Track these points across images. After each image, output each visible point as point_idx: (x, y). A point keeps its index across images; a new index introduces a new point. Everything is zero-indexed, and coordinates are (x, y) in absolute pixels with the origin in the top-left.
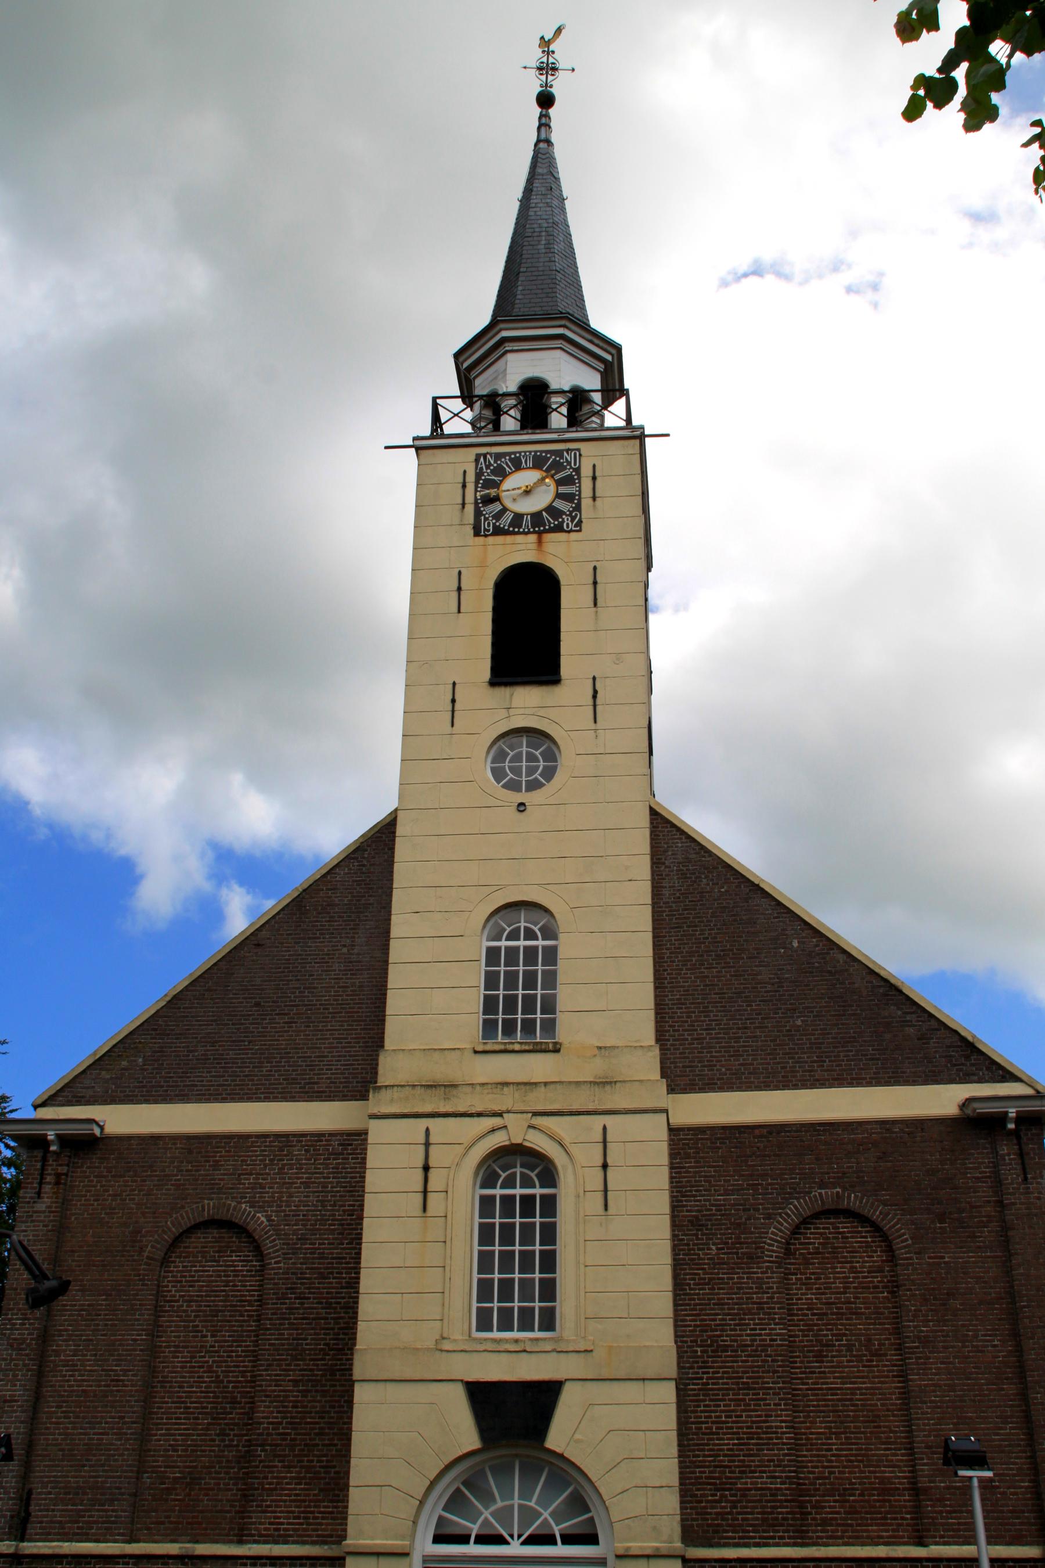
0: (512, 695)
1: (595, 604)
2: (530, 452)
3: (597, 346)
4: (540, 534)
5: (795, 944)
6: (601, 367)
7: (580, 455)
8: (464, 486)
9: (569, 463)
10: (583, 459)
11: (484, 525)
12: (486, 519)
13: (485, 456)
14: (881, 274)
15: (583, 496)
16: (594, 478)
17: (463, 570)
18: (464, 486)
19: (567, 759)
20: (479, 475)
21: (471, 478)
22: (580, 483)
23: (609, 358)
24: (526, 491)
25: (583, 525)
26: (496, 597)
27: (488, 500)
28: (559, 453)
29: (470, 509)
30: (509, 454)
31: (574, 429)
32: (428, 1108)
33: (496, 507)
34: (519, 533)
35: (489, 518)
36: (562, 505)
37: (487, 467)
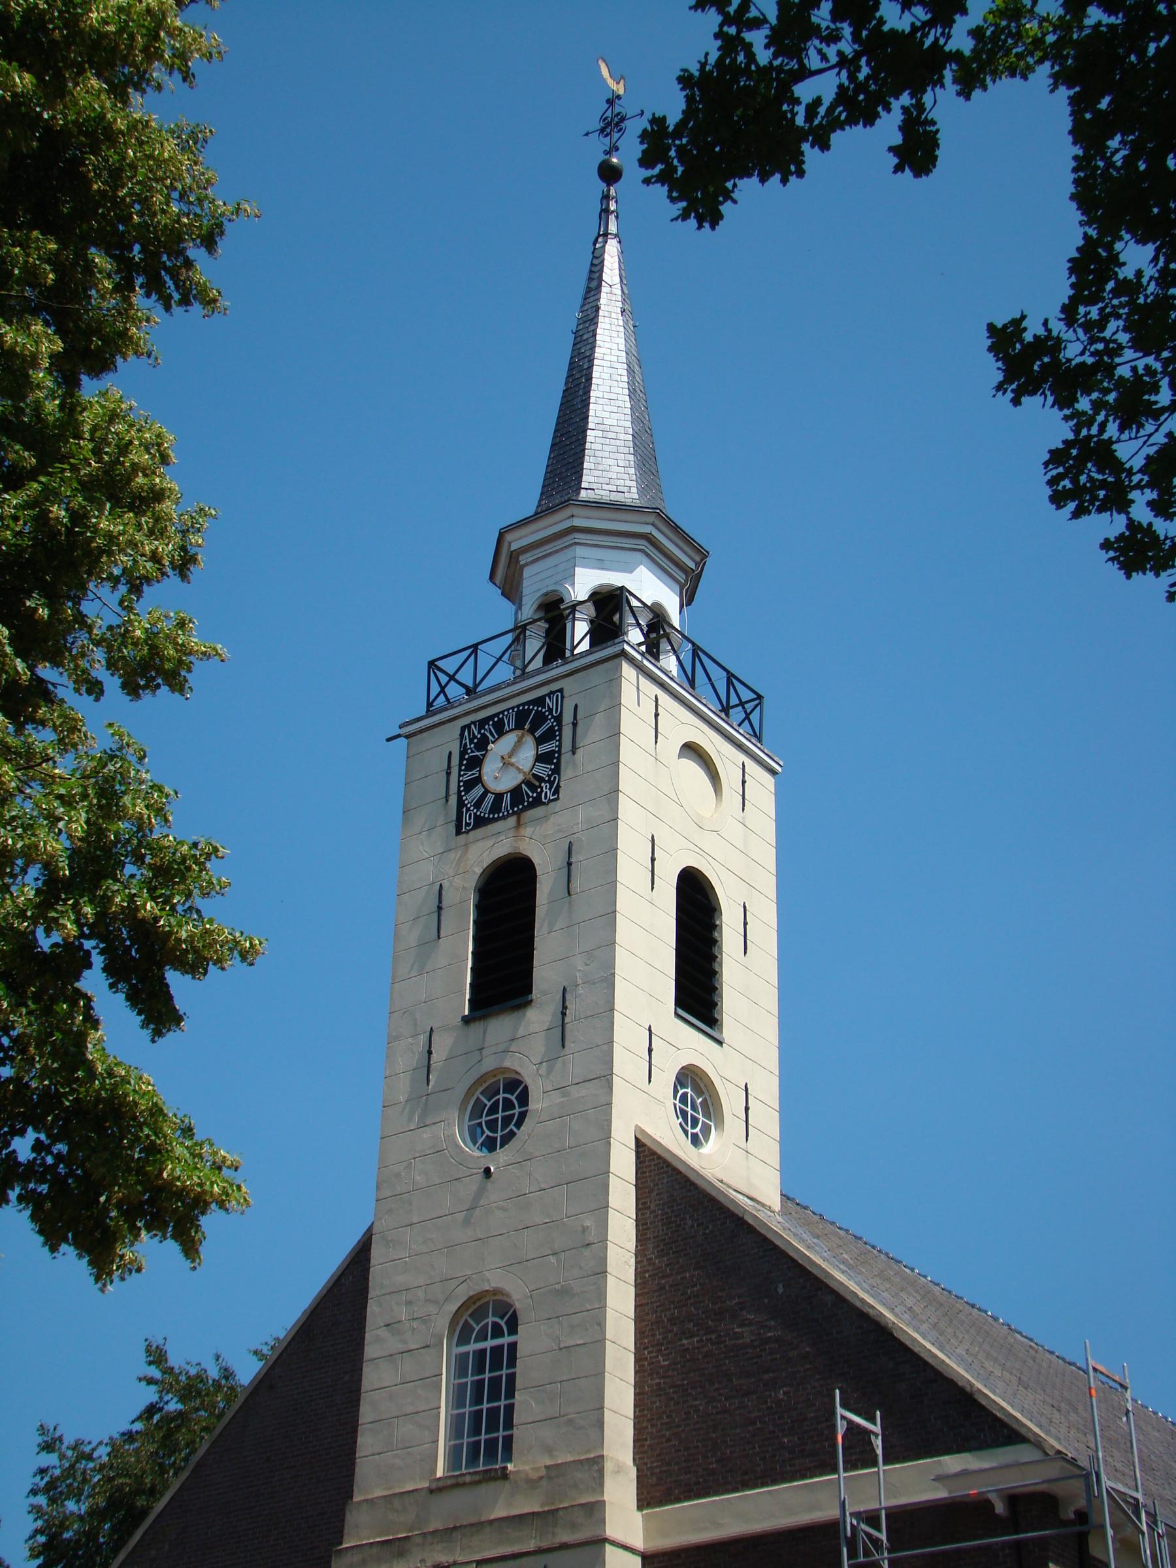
0: (485, 1031)
1: (569, 894)
2: (513, 708)
3: (686, 553)
4: (518, 814)
5: (780, 1290)
6: (681, 577)
7: (563, 697)
8: (448, 774)
9: (550, 710)
10: (565, 700)
11: (466, 818)
12: (468, 810)
13: (468, 726)
14: (210, 303)
15: (563, 751)
16: (575, 725)
17: (446, 884)
18: (448, 774)
19: (536, 1103)
20: (463, 753)
21: (455, 761)
22: (560, 735)
23: (692, 565)
24: (509, 762)
25: (561, 791)
26: (481, 908)
27: (470, 785)
28: (540, 701)
29: (453, 800)
30: (491, 717)
31: (551, 666)
32: (531, 1545)
33: (478, 791)
34: (499, 819)
35: (474, 811)
36: (543, 770)
37: (471, 742)
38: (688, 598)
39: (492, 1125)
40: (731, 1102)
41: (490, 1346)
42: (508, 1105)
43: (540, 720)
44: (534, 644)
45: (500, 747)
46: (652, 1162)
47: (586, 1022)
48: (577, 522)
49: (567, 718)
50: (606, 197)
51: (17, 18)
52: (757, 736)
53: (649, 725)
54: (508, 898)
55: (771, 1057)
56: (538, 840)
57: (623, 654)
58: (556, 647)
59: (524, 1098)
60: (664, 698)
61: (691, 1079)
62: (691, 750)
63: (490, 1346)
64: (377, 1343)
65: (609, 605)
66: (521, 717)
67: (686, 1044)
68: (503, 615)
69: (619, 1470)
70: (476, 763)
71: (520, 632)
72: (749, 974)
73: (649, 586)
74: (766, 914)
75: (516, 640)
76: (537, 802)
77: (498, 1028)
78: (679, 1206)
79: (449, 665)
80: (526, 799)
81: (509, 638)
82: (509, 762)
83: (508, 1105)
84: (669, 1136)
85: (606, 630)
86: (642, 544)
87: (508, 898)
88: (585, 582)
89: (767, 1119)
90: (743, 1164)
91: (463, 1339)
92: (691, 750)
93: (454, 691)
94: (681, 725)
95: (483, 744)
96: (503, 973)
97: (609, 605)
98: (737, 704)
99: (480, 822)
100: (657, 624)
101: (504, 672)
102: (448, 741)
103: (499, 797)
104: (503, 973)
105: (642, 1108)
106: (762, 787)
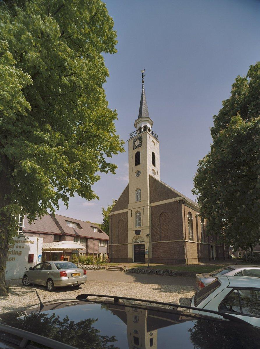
24: (137, 143)
35: (135, 147)
36: (140, 143)
38: (151, 127)
39: (138, 175)
40: (156, 172)
41: (138, 192)
42: (139, 173)
43: (140, 139)
44: (139, 132)
45: (138, 144)
46: (150, 176)
47: (145, 166)
48: (142, 119)
49: (142, 138)
50: (143, 85)
51: (24, 19)
52: (158, 140)
53: (149, 138)
54: (138, 155)
55: (159, 168)
56: (139, 149)
57: (147, 132)
58: (140, 132)
59: (140, 172)
60: (150, 136)
61: (153, 170)
62: (152, 141)
63: (138, 192)
64: (129, 190)
65: (145, 127)
66: (138, 138)
67: (153, 167)
68: (136, 129)
69: (169, 307)
70: (134, 143)
71: (137, 130)
72: (157, 161)
73: (149, 126)
74: (159, 158)
75: (137, 132)
76: (140, 146)
77: (138, 166)
78: (152, 179)
79: (131, 134)
80: (139, 146)
81: (136, 132)
82: (137, 143)
83: (139, 173)
84: (152, 175)
85: (145, 130)
86: (148, 121)
87: (138, 155)
88: (143, 126)
89: (159, 173)
90: (158, 177)
91: (136, 191)
92: (152, 141)
93: (132, 137)
94: (152, 139)
95: (135, 141)
96: (138, 161)
97: (145, 127)
98: (156, 137)
99: (135, 149)
100: (149, 129)
101: (136, 135)
102: (132, 141)
103: (137, 146)
104: (138, 161)
105: (150, 173)
106: (158, 144)
